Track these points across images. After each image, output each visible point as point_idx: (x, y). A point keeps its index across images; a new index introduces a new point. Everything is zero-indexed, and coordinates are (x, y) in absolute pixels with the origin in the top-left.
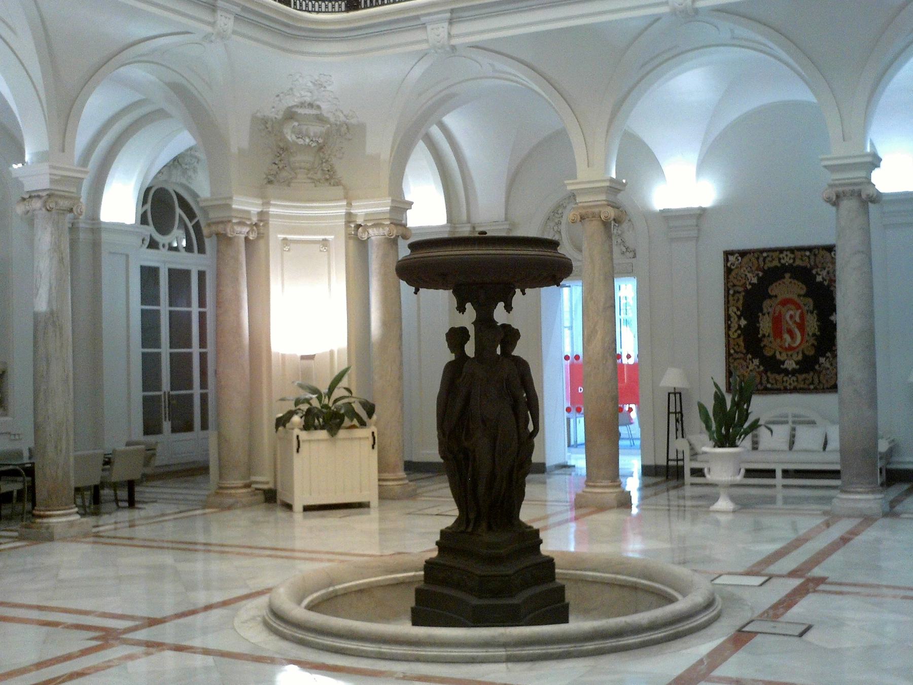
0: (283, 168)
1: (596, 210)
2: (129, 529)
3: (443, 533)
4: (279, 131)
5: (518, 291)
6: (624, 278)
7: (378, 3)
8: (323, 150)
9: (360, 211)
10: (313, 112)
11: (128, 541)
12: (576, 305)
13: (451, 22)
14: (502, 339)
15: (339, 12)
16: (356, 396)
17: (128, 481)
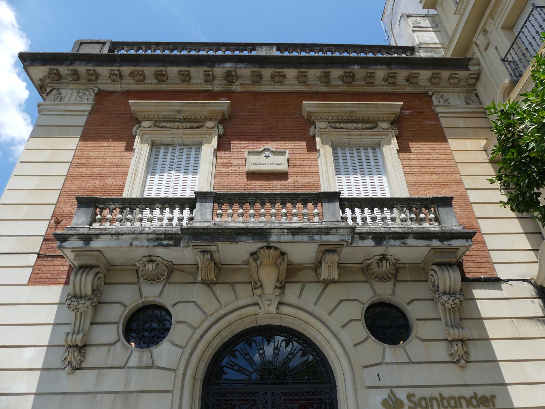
2: (499, 59)
3: (390, 145)
4: (517, 69)
5: (360, 210)
6: (446, 70)
9: (406, 112)
11: (434, 45)
12: (108, 230)
14: (209, 284)
17: (461, 282)
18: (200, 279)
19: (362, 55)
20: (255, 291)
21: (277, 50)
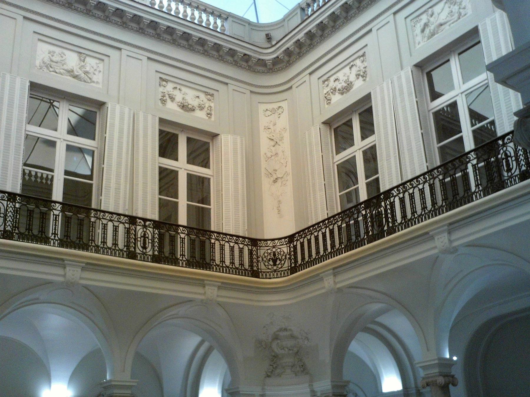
0: (276, 367)
1: (434, 379)
7: (512, 184)
8: (298, 354)
10: (288, 333)
13: (335, 275)
15: (280, 277)
16: (185, 224)
18: (91, 223)
19: (384, 216)
20: (204, 107)
21: (288, 258)
